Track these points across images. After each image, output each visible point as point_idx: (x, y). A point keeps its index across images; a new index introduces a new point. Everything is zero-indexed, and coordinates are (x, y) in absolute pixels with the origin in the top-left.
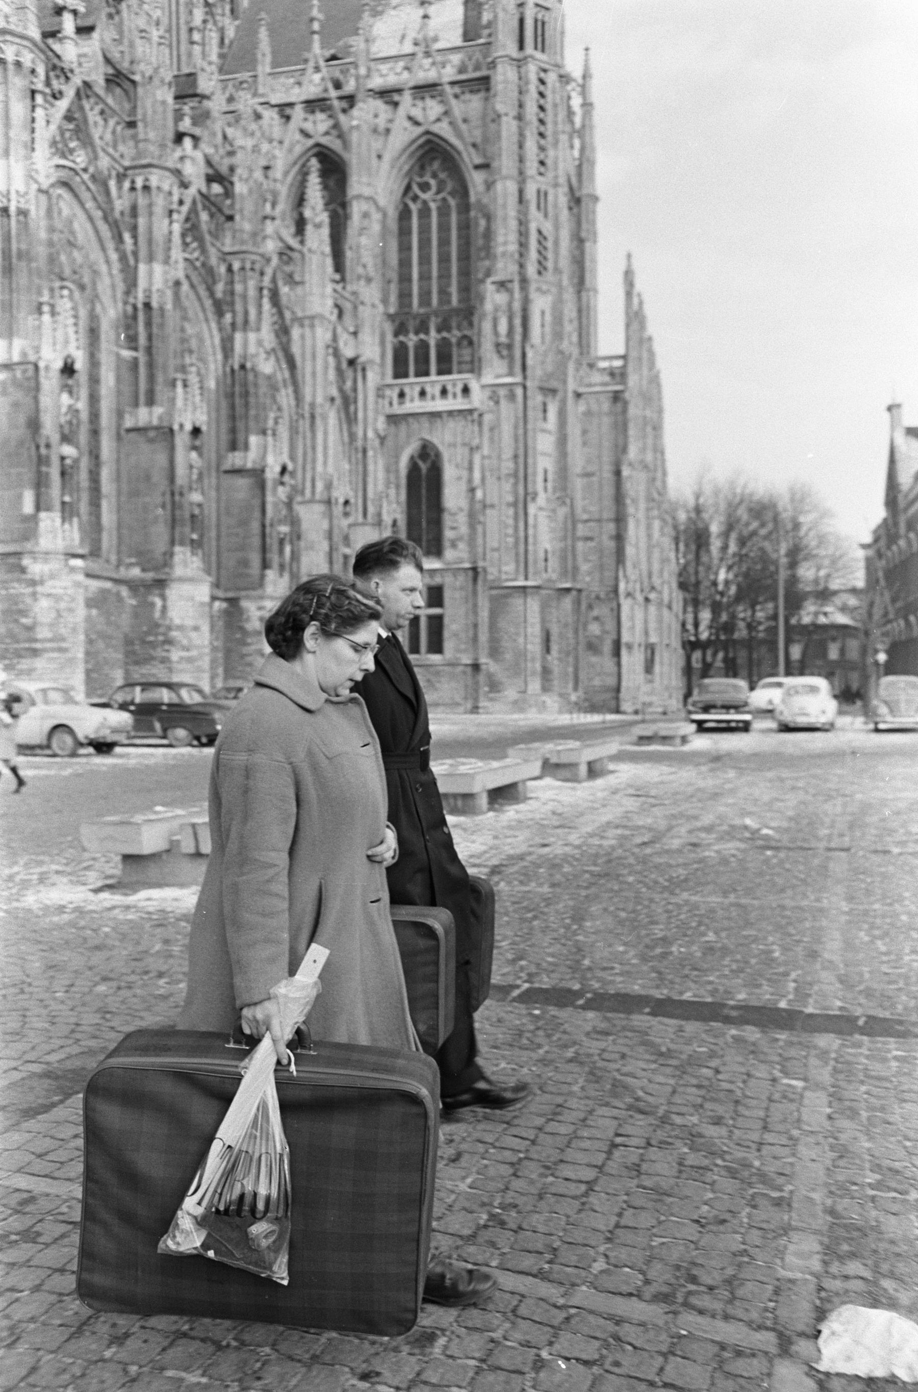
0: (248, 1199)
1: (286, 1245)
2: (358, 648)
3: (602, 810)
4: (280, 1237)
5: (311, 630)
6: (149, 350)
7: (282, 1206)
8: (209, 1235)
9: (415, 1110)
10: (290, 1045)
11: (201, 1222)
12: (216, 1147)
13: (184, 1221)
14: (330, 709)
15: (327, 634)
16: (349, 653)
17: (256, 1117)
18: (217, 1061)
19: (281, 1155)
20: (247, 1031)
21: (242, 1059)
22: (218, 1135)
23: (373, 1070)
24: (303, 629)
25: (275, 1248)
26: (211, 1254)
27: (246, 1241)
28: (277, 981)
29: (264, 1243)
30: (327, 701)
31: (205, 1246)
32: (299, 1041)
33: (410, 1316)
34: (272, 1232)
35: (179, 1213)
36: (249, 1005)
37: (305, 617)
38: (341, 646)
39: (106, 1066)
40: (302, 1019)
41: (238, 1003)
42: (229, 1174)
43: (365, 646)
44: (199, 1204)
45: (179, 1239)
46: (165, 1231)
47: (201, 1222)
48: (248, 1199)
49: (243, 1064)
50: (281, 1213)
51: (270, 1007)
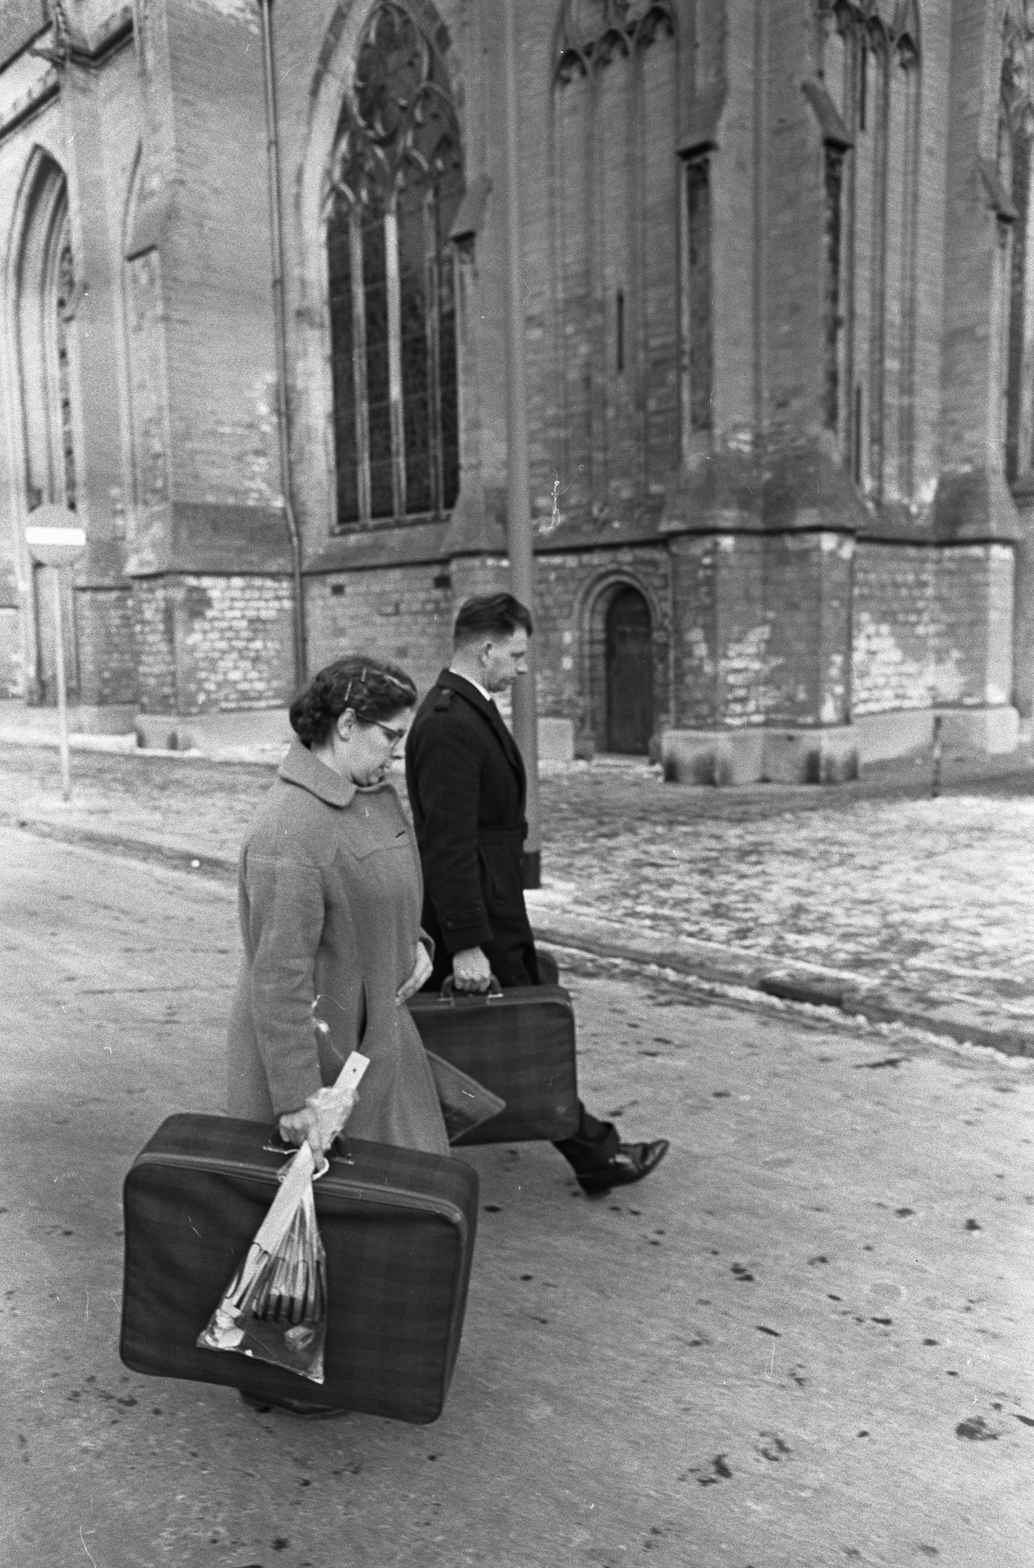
0: (285, 1304)
1: (321, 1346)
2: (391, 735)
3: (963, 955)
4: (316, 1340)
5: (348, 714)
6: (240, 709)
7: (318, 1310)
8: (246, 1337)
9: (450, 1231)
10: (328, 1154)
11: (238, 1323)
12: (253, 1252)
13: (227, 1313)
14: (362, 799)
15: (364, 719)
16: (382, 740)
17: (293, 1223)
18: (251, 1166)
19: (318, 1263)
20: (286, 1139)
21: (279, 1167)
22: (257, 1240)
23: (410, 1187)
24: (337, 716)
25: (311, 1350)
26: (249, 1353)
27: (281, 1342)
28: (314, 1091)
29: (301, 1345)
30: (357, 792)
31: (243, 1345)
32: (337, 1149)
33: (434, 1410)
34: (308, 1336)
35: (218, 1312)
36: (287, 1113)
37: (335, 706)
38: (375, 733)
39: (140, 1162)
40: (339, 1129)
41: (276, 1110)
42: (268, 1275)
43: (400, 733)
44: (238, 1306)
45: (218, 1334)
46: (203, 1327)
47: (238, 1323)
48: (285, 1304)
49: (280, 1171)
50: (317, 1317)
51: (306, 1116)
